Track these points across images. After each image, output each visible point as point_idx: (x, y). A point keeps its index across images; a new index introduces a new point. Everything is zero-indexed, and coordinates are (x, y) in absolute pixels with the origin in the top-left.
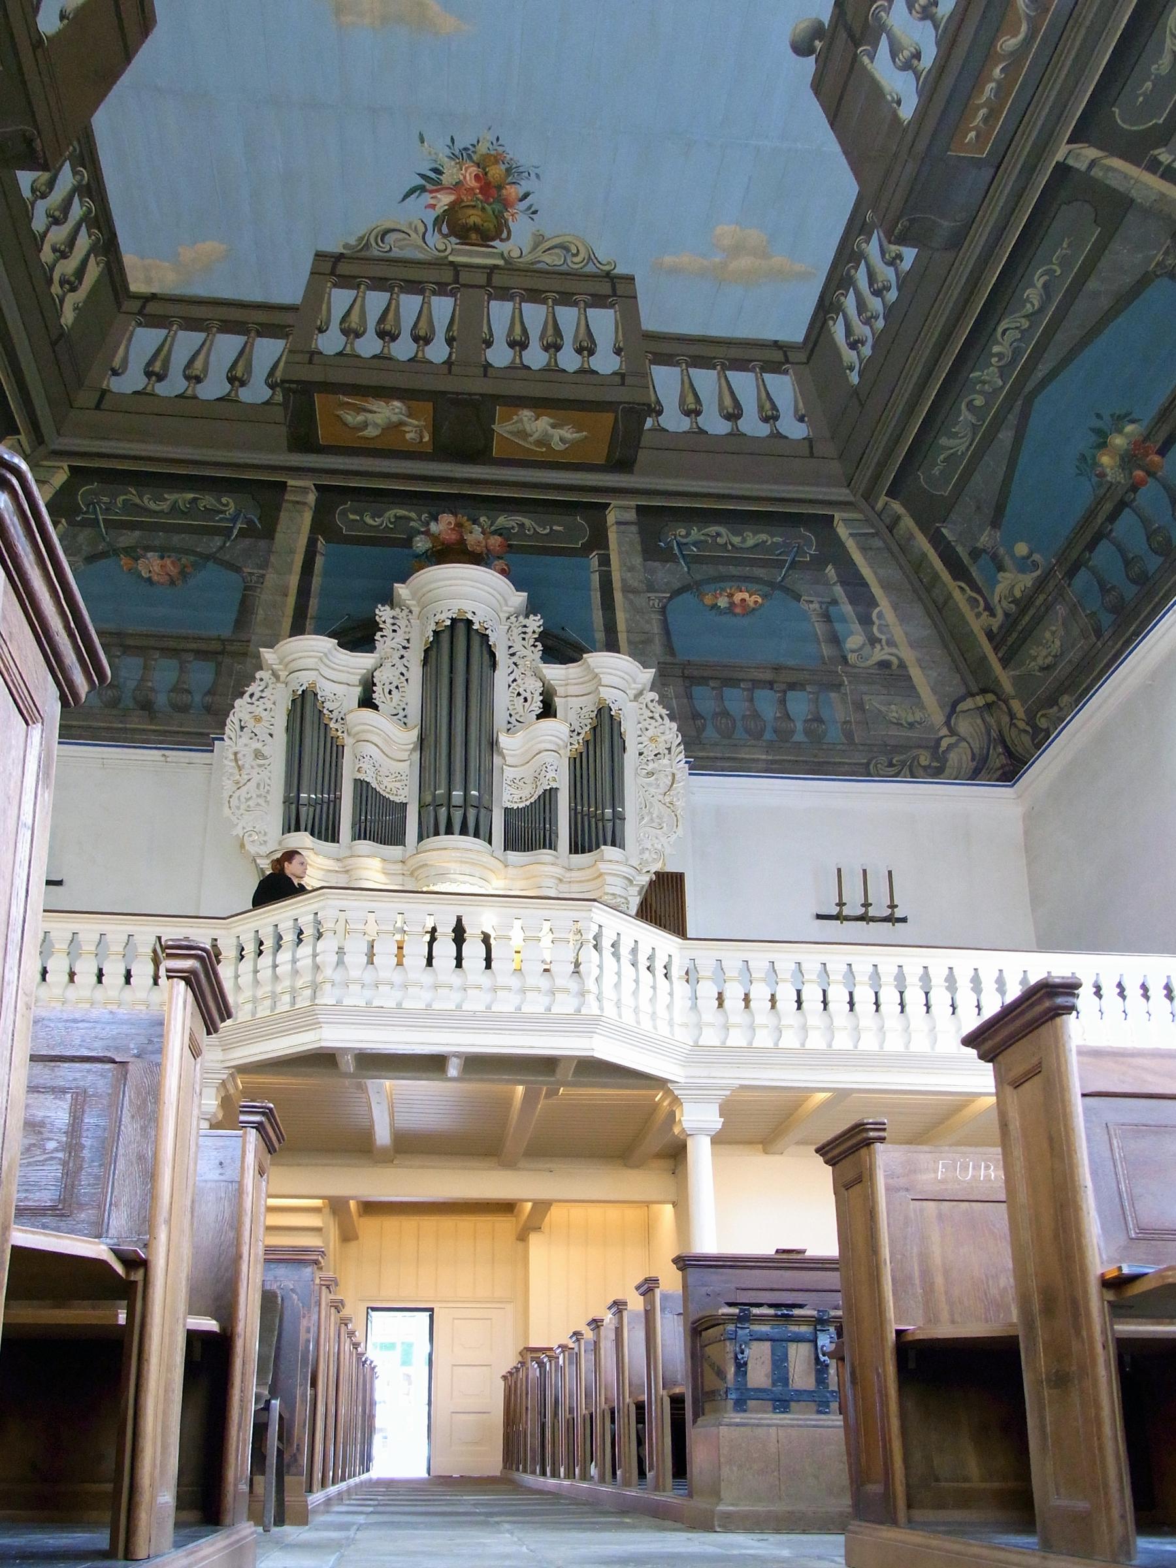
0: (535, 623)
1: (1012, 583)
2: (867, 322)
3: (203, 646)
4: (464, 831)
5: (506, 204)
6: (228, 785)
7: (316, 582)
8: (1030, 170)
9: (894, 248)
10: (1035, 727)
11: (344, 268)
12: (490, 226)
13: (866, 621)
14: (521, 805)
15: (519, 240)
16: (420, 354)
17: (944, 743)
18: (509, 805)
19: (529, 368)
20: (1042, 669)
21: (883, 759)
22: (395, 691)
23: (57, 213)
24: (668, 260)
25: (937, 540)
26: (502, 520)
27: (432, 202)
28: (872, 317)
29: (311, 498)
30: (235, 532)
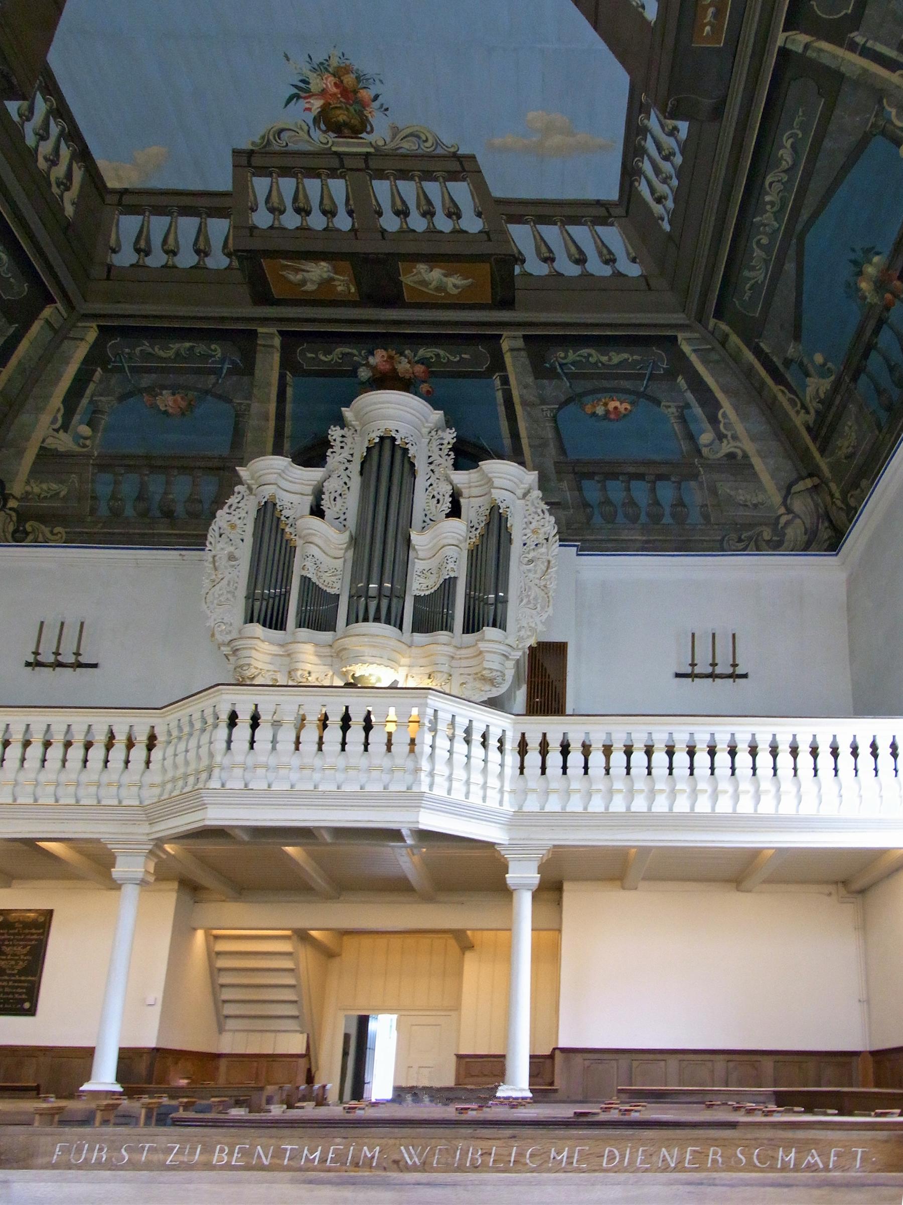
0: (449, 436)
1: (817, 386)
2: (665, 181)
3: (210, 464)
4: (377, 619)
5: (363, 105)
6: (206, 583)
7: (289, 408)
8: (759, 54)
9: (670, 123)
10: (848, 505)
11: (257, 161)
12: (355, 122)
13: (713, 420)
14: (427, 593)
15: (380, 133)
16: (330, 225)
17: (783, 520)
18: (418, 593)
19: (414, 231)
20: (846, 458)
21: (734, 536)
22: (338, 498)
23: (41, 131)
24: (497, 141)
25: (758, 352)
26: (422, 352)
27: (307, 106)
28: (667, 178)
29: (277, 341)
30: (225, 371)
